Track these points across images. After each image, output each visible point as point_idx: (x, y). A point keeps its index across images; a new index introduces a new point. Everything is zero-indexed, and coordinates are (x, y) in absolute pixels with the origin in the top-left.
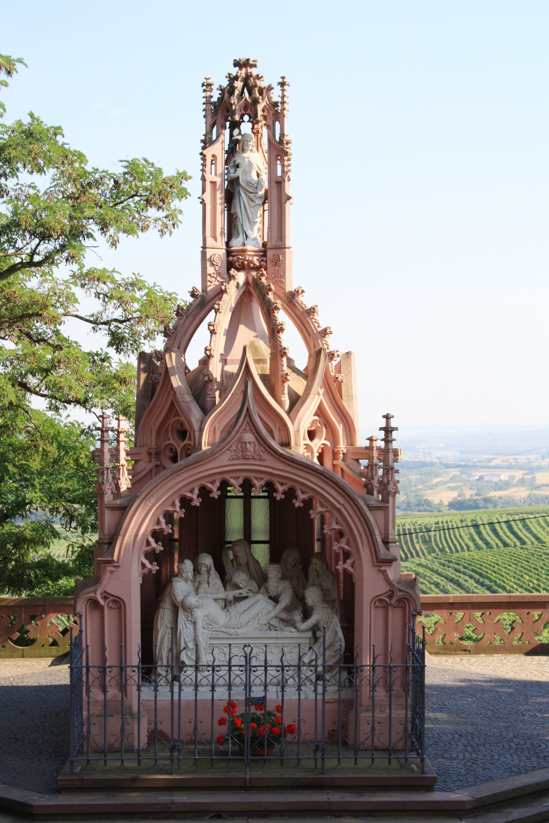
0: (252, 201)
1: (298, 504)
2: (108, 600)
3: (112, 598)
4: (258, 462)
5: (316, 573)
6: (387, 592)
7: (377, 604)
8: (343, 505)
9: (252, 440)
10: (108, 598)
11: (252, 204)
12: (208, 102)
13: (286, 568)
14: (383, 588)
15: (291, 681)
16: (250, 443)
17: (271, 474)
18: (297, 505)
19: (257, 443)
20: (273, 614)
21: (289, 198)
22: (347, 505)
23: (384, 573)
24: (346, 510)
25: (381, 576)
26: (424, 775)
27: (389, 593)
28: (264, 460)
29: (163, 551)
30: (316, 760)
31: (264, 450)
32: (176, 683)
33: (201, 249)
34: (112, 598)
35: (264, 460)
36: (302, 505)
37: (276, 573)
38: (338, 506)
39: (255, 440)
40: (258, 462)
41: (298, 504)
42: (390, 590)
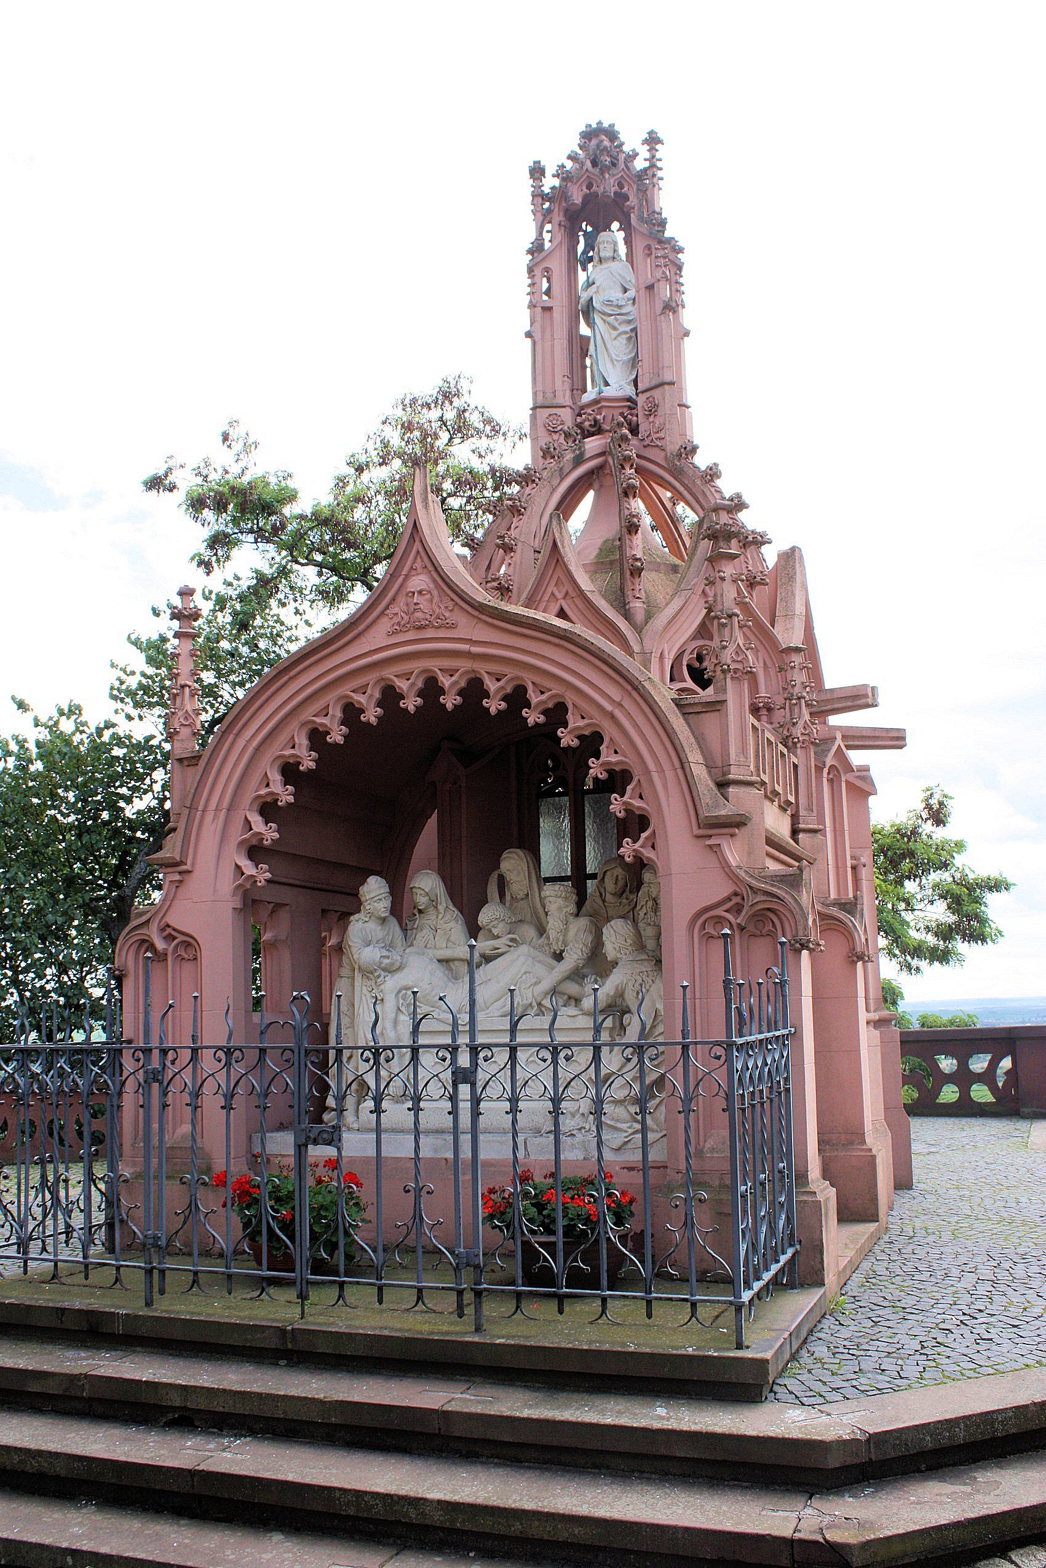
0: (615, 329)
1: (533, 717)
2: (176, 942)
3: (181, 938)
4: (441, 634)
5: (650, 903)
6: (729, 899)
7: (709, 929)
8: (620, 705)
9: (425, 587)
10: (174, 938)
11: (615, 333)
12: (539, 196)
13: (604, 901)
14: (719, 889)
15: (435, 1089)
16: (420, 592)
17: (469, 655)
18: (531, 721)
19: (435, 593)
20: (546, 984)
21: (687, 334)
22: (627, 703)
23: (715, 849)
24: (636, 726)
25: (711, 861)
26: (740, 1354)
27: (736, 900)
28: (453, 626)
29: (277, 839)
30: (460, 1293)
31: (450, 604)
32: (156, 1086)
33: (531, 412)
34: (181, 938)
35: (453, 626)
36: (542, 719)
37: (560, 901)
38: (608, 707)
39: (432, 586)
40: (441, 634)
41: (533, 717)
42: (736, 894)
